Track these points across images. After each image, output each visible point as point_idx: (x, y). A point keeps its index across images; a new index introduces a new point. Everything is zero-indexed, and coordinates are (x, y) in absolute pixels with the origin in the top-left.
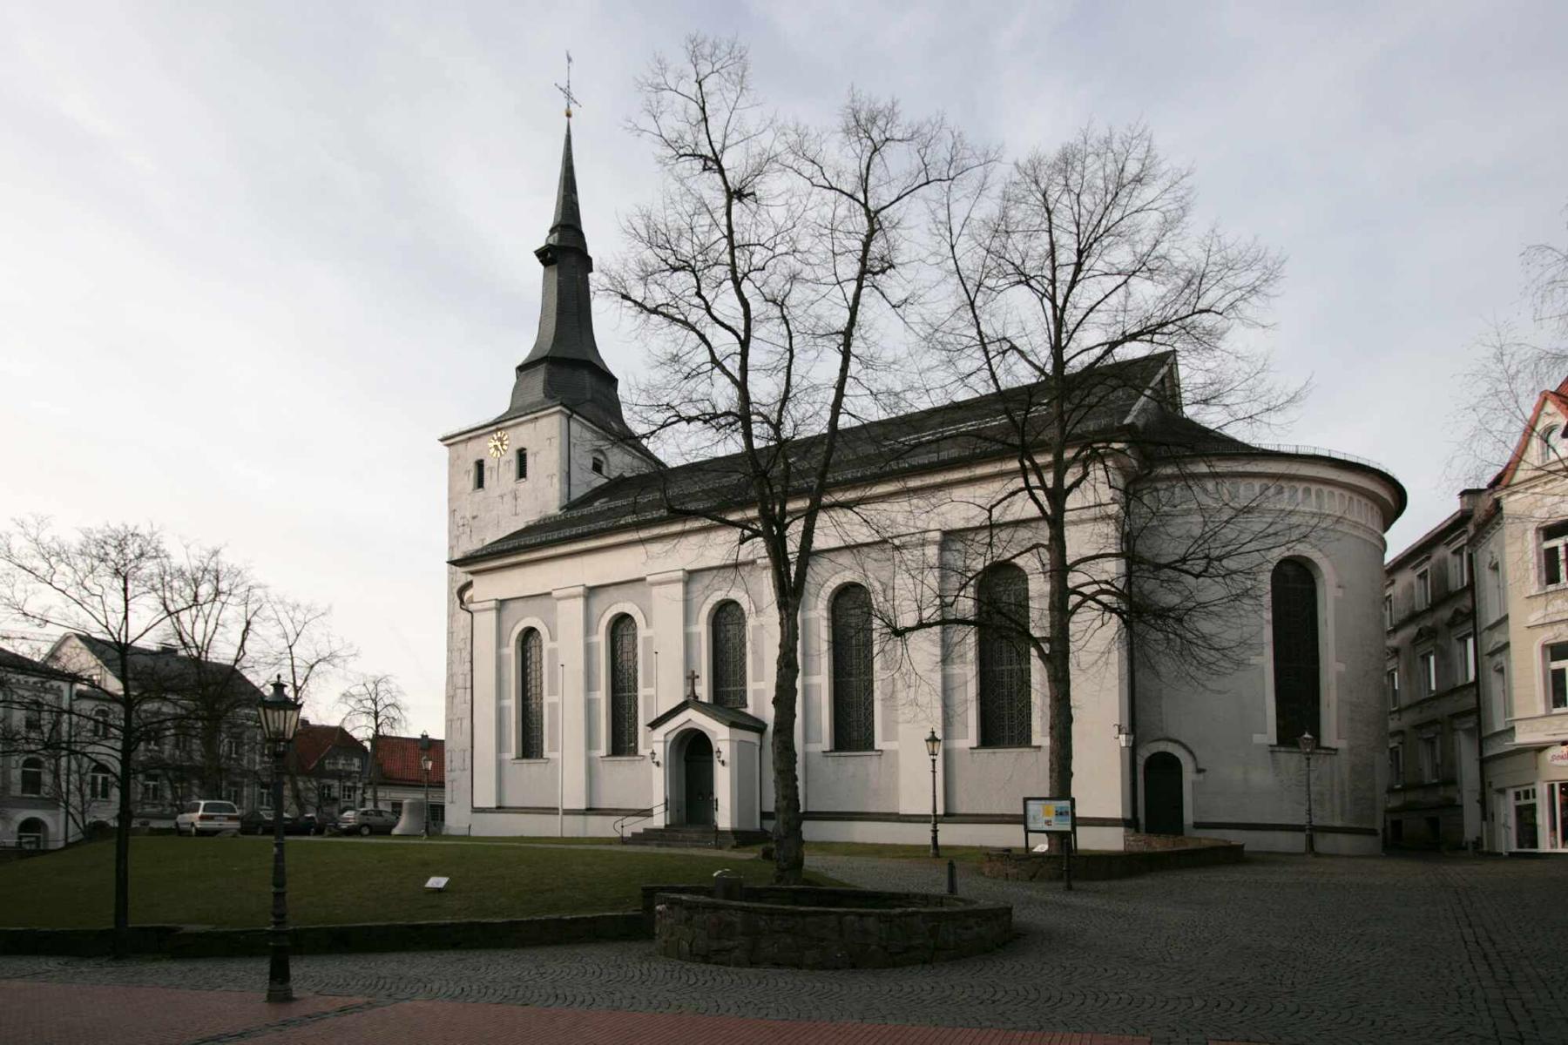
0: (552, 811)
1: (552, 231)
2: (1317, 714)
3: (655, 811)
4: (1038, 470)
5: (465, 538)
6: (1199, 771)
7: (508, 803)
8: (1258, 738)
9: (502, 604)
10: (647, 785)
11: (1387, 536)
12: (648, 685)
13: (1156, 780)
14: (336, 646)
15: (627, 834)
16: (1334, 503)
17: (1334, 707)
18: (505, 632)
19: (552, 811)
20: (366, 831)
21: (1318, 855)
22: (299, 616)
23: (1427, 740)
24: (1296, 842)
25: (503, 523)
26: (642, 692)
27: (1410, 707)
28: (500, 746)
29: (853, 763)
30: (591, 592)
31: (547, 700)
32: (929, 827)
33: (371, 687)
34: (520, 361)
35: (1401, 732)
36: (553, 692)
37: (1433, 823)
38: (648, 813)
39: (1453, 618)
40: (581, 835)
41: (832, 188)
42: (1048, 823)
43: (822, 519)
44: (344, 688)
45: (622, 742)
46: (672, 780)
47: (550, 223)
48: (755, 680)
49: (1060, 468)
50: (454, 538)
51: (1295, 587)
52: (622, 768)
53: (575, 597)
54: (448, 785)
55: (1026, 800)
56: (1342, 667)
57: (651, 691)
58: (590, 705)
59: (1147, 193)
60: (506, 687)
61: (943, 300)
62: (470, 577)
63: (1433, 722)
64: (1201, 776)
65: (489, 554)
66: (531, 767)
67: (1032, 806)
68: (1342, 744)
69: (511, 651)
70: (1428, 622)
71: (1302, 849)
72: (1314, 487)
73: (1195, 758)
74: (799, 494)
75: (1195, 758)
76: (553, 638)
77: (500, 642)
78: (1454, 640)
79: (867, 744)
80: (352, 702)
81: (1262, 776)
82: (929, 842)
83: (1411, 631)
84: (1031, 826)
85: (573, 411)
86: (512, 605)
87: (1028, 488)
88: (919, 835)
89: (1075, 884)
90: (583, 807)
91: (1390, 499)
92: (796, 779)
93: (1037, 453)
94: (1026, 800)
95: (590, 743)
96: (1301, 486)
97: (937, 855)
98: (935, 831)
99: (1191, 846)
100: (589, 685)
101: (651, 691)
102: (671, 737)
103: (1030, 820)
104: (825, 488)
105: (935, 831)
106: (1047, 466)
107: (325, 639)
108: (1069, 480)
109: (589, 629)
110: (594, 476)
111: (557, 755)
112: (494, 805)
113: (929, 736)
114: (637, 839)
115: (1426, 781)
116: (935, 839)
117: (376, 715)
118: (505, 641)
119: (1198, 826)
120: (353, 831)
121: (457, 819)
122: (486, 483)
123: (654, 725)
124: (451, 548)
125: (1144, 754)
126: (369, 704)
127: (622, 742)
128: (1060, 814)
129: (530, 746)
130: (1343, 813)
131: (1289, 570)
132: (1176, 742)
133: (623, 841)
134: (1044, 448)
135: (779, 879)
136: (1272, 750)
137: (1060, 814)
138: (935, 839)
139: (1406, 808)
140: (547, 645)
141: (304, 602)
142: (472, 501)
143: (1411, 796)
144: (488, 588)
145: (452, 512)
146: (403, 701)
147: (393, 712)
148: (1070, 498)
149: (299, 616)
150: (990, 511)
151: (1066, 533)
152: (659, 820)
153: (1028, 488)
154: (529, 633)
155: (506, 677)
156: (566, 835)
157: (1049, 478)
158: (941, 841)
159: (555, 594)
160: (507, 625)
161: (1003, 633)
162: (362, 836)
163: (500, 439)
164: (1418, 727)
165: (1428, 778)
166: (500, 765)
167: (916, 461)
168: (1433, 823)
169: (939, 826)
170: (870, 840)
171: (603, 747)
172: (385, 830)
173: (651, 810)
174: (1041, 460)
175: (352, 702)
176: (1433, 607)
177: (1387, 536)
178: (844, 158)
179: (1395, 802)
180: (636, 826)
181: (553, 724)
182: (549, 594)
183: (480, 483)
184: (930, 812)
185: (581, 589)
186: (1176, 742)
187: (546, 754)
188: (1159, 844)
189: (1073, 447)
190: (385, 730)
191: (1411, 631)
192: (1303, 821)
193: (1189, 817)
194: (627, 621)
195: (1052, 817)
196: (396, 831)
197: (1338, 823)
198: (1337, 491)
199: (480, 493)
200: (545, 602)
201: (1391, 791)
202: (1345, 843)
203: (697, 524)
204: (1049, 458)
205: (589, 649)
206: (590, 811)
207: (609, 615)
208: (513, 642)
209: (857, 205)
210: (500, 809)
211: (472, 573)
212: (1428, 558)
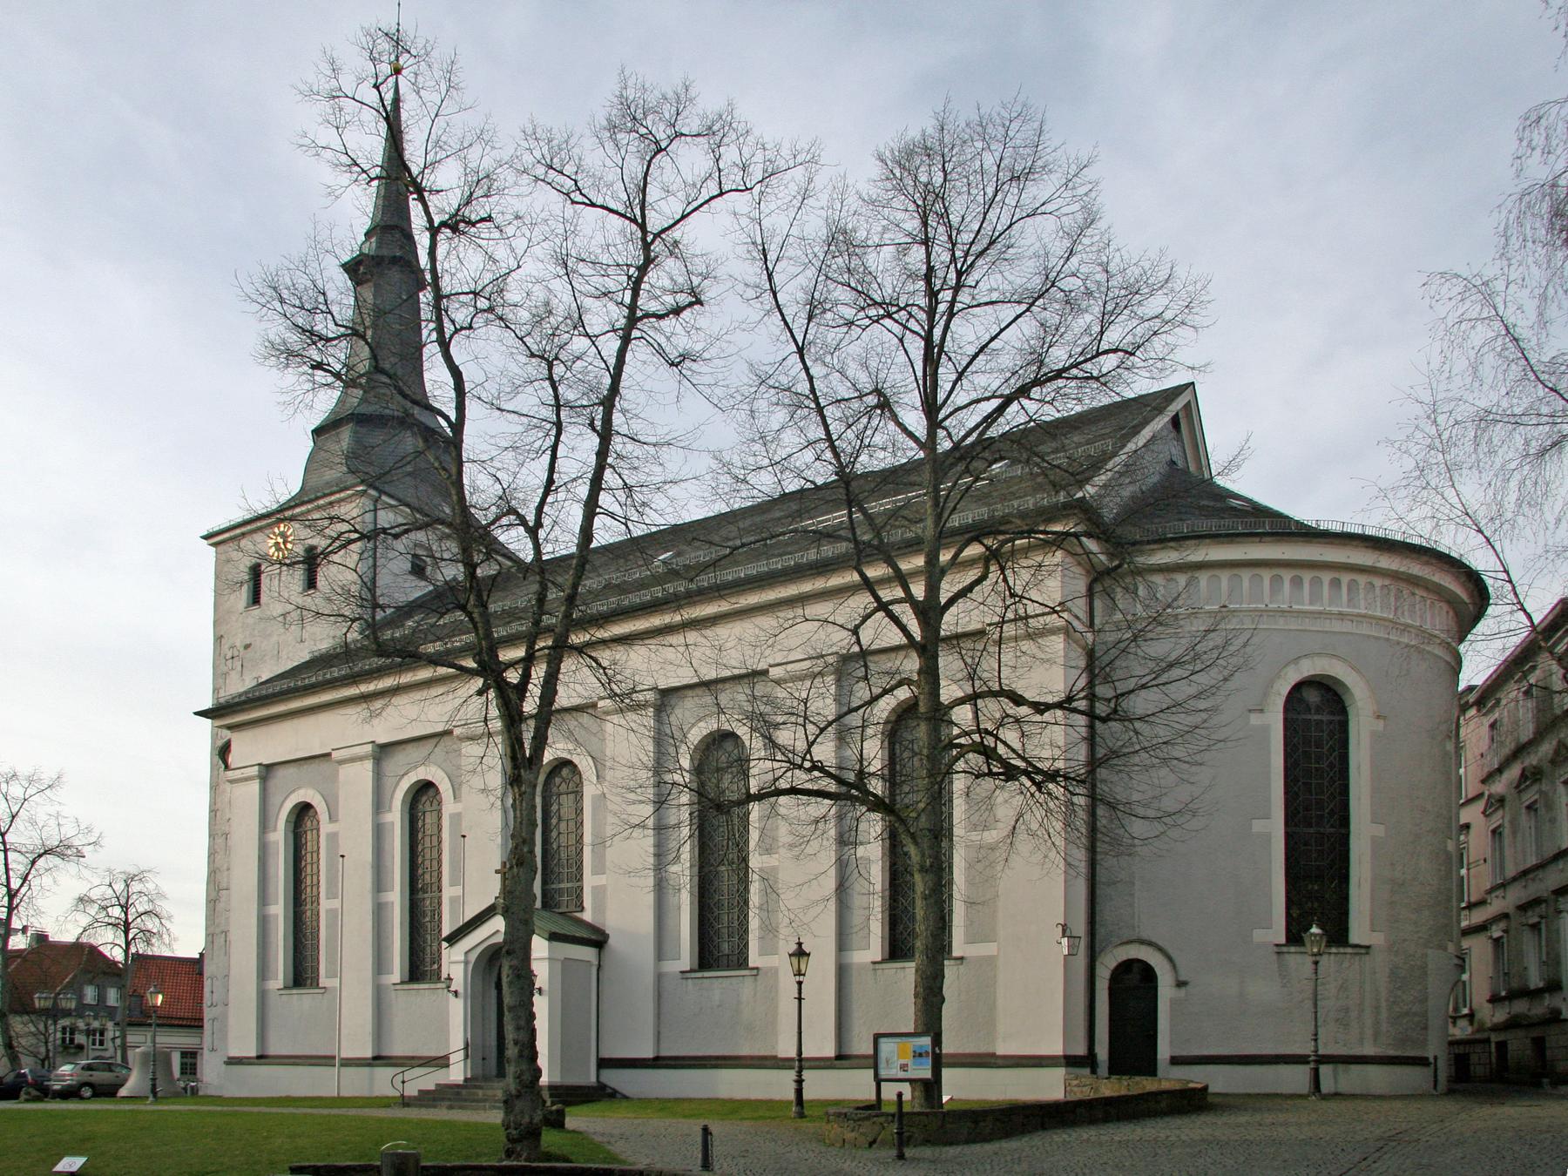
0: (326, 1060)
1: (368, 235)
2: (1345, 898)
3: (453, 1058)
4: (902, 579)
5: (234, 676)
6: (1181, 984)
7: (273, 1049)
8: (1259, 935)
9: (267, 771)
10: (446, 1023)
11: (1462, 648)
12: (332, 895)
13: (1127, 1005)
14: (69, 831)
15: (412, 1090)
16: (1371, 601)
17: (1366, 888)
18: (272, 810)
19: (326, 1060)
20: (87, 1092)
21: (1325, 1097)
22: (16, 790)
23: (1535, 927)
24: (1296, 1078)
25: (284, 654)
26: (448, 892)
27: (1514, 879)
28: (263, 972)
29: (719, 984)
30: (383, 751)
31: (325, 904)
32: (791, 1075)
33: (119, 887)
34: (316, 422)
35: (1505, 916)
36: (599, 869)
37: (1539, 1043)
38: (442, 1062)
39: (1557, 752)
40: (366, 1093)
41: (593, 205)
42: (904, 1067)
43: (568, 664)
44: (81, 889)
45: (420, 968)
46: (475, 1018)
47: (366, 223)
48: (594, 873)
49: (934, 574)
50: (220, 675)
51: (1317, 718)
52: (413, 1003)
53: (361, 759)
54: (207, 1025)
55: (877, 1037)
56: (1380, 831)
57: (336, 903)
58: (379, 910)
59: (1035, 192)
60: (271, 889)
61: (767, 345)
62: (227, 734)
63: (1537, 902)
64: (1182, 992)
65: (245, 702)
66: (303, 1000)
67: (886, 1046)
68: (1376, 939)
69: (279, 836)
70: (1532, 760)
71: (1305, 1091)
72: (1345, 578)
73: (1174, 966)
74: (510, 641)
75: (1174, 966)
76: (456, 797)
77: (265, 825)
78: (1558, 783)
79: (739, 961)
80: (93, 909)
81: (1264, 989)
82: (791, 1096)
83: (1514, 772)
84: (883, 1073)
85: (381, 492)
86: (281, 773)
87: (883, 606)
88: (779, 1085)
89: (908, 1152)
90: (369, 1054)
91: (1464, 596)
92: (532, 1016)
93: (869, 563)
94: (877, 1037)
95: (380, 966)
96: (1326, 577)
97: (801, 1115)
98: (800, 1082)
99: (1165, 1085)
100: (379, 885)
101: (336, 903)
102: (473, 956)
103: (882, 1065)
104: (571, 624)
105: (800, 1082)
106: (915, 573)
107: (53, 822)
108: (947, 590)
109: (379, 805)
110: (413, 581)
111: (335, 983)
112: (253, 1054)
113: (794, 947)
114: (427, 1099)
115: (1532, 987)
116: (799, 1092)
117: (127, 926)
118: (271, 824)
119: (1175, 1061)
120: (69, 1093)
121: (211, 1072)
122: (264, 598)
123: (453, 938)
124: (216, 690)
125: (1108, 964)
126: (117, 912)
127: (420, 968)
128: (918, 1055)
129: (302, 975)
130: (1376, 1035)
131: (1312, 697)
132: (1150, 944)
133: (405, 1102)
134: (912, 546)
135: (509, 1154)
136: (1279, 950)
137: (918, 1055)
138: (799, 1092)
139: (1513, 1024)
140: (326, 828)
141: (24, 770)
142: (246, 623)
143: (1520, 1006)
144: (252, 748)
145: (219, 639)
146: (164, 907)
147: (151, 924)
148: (948, 617)
149: (16, 790)
150: (855, 631)
151: (941, 662)
152: (456, 1073)
153: (883, 606)
154: (304, 810)
155: (272, 871)
156: (344, 1093)
157: (918, 590)
158: (807, 1095)
159: (335, 755)
160: (274, 800)
161: (907, 805)
162: (82, 1098)
163: (283, 535)
164: (1523, 908)
165: (1535, 980)
166: (262, 995)
167: (729, 575)
168: (1539, 1043)
169: (806, 1074)
170: (739, 1094)
171: (278, 980)
172: (107, 1091)
173: (446, 1057)
174: (873, 572)
175: (93, 910)
176: (1540, 736)
177: (1462, 648)
178: (607, 166)
179: (1501, 1015)
180: (422, 1081)
181: (332, 938)
182: (328, 755)
183: (255, 599)
184: (793, 1054)
185: (369, 748)
186: (1150, 944)
187: (323, 981)
188: (1110, 1088)
189: (947, 546)
190: (139, 947)
191: (1514, 772)
192: (1306, 1049)
193: (1164, 1051)
194: (431, 792)
195: (909, 1060)
196: (123, 1092)
197: (1369, 1050)
198: (1378, 582)
199: (256, 612)
200: (324, 766)
201: (1494, 999)
202: (1377, 1078)
203: (425, 674)
204: (919, 561)
205: (379, 832)
206: (378, 1060)
207: (405, 784)
208: (281, 824)
209: (634, 227)
210: (262, 1058)
211: (230, 727)
212: (1534, 668)
